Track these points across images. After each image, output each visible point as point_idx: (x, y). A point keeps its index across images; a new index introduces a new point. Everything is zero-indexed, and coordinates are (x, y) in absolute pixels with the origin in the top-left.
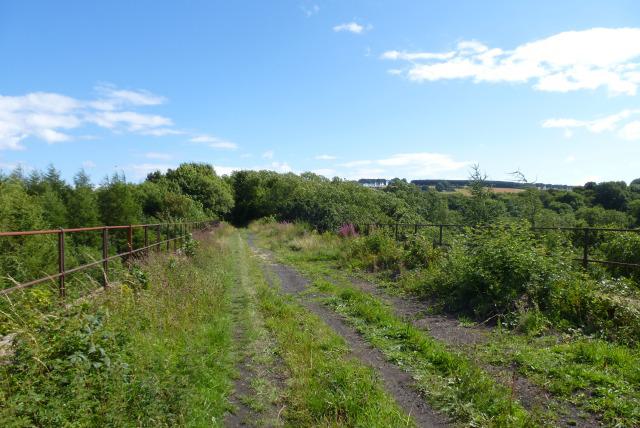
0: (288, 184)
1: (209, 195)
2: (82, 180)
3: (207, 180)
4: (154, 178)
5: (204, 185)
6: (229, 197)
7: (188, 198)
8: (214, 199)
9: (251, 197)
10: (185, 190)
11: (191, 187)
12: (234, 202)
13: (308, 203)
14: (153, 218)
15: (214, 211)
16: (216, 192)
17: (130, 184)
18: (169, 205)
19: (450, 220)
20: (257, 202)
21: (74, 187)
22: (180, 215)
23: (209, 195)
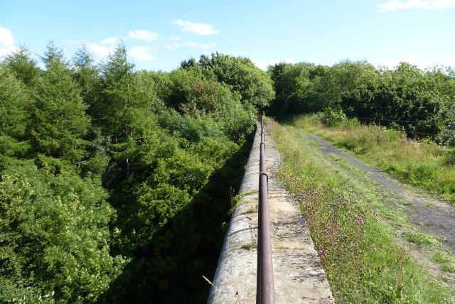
0: (447, 74)
1: (246, 85)
2: (51, 58)
3: (245, 68)
4: (187, 65)
5: (242, 73)
6: (269, 86)
7: (226, 89)
8: (252, 90)
9: (292, 90)
10: (220, 79)
11: (227, 75)
12: (274, 93)
13: (371, 88)
14: (174, 111)
15: (253, 104)
16: (255, 81)
17: (38, 69)
18: (197, 94)
19: (85, 271)
20: (300, 94)
21: (42, 66)
22: (210, 108)
23: (246, 85)
